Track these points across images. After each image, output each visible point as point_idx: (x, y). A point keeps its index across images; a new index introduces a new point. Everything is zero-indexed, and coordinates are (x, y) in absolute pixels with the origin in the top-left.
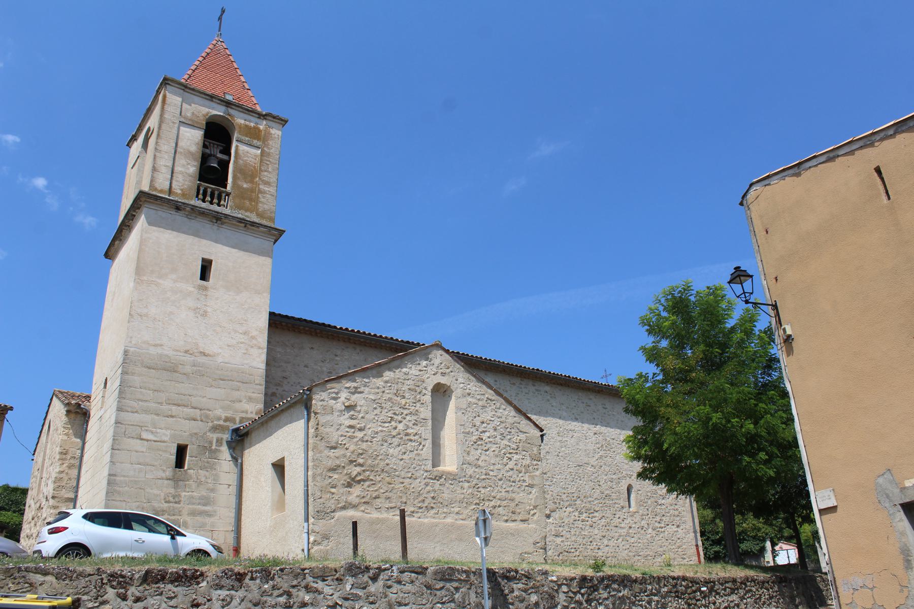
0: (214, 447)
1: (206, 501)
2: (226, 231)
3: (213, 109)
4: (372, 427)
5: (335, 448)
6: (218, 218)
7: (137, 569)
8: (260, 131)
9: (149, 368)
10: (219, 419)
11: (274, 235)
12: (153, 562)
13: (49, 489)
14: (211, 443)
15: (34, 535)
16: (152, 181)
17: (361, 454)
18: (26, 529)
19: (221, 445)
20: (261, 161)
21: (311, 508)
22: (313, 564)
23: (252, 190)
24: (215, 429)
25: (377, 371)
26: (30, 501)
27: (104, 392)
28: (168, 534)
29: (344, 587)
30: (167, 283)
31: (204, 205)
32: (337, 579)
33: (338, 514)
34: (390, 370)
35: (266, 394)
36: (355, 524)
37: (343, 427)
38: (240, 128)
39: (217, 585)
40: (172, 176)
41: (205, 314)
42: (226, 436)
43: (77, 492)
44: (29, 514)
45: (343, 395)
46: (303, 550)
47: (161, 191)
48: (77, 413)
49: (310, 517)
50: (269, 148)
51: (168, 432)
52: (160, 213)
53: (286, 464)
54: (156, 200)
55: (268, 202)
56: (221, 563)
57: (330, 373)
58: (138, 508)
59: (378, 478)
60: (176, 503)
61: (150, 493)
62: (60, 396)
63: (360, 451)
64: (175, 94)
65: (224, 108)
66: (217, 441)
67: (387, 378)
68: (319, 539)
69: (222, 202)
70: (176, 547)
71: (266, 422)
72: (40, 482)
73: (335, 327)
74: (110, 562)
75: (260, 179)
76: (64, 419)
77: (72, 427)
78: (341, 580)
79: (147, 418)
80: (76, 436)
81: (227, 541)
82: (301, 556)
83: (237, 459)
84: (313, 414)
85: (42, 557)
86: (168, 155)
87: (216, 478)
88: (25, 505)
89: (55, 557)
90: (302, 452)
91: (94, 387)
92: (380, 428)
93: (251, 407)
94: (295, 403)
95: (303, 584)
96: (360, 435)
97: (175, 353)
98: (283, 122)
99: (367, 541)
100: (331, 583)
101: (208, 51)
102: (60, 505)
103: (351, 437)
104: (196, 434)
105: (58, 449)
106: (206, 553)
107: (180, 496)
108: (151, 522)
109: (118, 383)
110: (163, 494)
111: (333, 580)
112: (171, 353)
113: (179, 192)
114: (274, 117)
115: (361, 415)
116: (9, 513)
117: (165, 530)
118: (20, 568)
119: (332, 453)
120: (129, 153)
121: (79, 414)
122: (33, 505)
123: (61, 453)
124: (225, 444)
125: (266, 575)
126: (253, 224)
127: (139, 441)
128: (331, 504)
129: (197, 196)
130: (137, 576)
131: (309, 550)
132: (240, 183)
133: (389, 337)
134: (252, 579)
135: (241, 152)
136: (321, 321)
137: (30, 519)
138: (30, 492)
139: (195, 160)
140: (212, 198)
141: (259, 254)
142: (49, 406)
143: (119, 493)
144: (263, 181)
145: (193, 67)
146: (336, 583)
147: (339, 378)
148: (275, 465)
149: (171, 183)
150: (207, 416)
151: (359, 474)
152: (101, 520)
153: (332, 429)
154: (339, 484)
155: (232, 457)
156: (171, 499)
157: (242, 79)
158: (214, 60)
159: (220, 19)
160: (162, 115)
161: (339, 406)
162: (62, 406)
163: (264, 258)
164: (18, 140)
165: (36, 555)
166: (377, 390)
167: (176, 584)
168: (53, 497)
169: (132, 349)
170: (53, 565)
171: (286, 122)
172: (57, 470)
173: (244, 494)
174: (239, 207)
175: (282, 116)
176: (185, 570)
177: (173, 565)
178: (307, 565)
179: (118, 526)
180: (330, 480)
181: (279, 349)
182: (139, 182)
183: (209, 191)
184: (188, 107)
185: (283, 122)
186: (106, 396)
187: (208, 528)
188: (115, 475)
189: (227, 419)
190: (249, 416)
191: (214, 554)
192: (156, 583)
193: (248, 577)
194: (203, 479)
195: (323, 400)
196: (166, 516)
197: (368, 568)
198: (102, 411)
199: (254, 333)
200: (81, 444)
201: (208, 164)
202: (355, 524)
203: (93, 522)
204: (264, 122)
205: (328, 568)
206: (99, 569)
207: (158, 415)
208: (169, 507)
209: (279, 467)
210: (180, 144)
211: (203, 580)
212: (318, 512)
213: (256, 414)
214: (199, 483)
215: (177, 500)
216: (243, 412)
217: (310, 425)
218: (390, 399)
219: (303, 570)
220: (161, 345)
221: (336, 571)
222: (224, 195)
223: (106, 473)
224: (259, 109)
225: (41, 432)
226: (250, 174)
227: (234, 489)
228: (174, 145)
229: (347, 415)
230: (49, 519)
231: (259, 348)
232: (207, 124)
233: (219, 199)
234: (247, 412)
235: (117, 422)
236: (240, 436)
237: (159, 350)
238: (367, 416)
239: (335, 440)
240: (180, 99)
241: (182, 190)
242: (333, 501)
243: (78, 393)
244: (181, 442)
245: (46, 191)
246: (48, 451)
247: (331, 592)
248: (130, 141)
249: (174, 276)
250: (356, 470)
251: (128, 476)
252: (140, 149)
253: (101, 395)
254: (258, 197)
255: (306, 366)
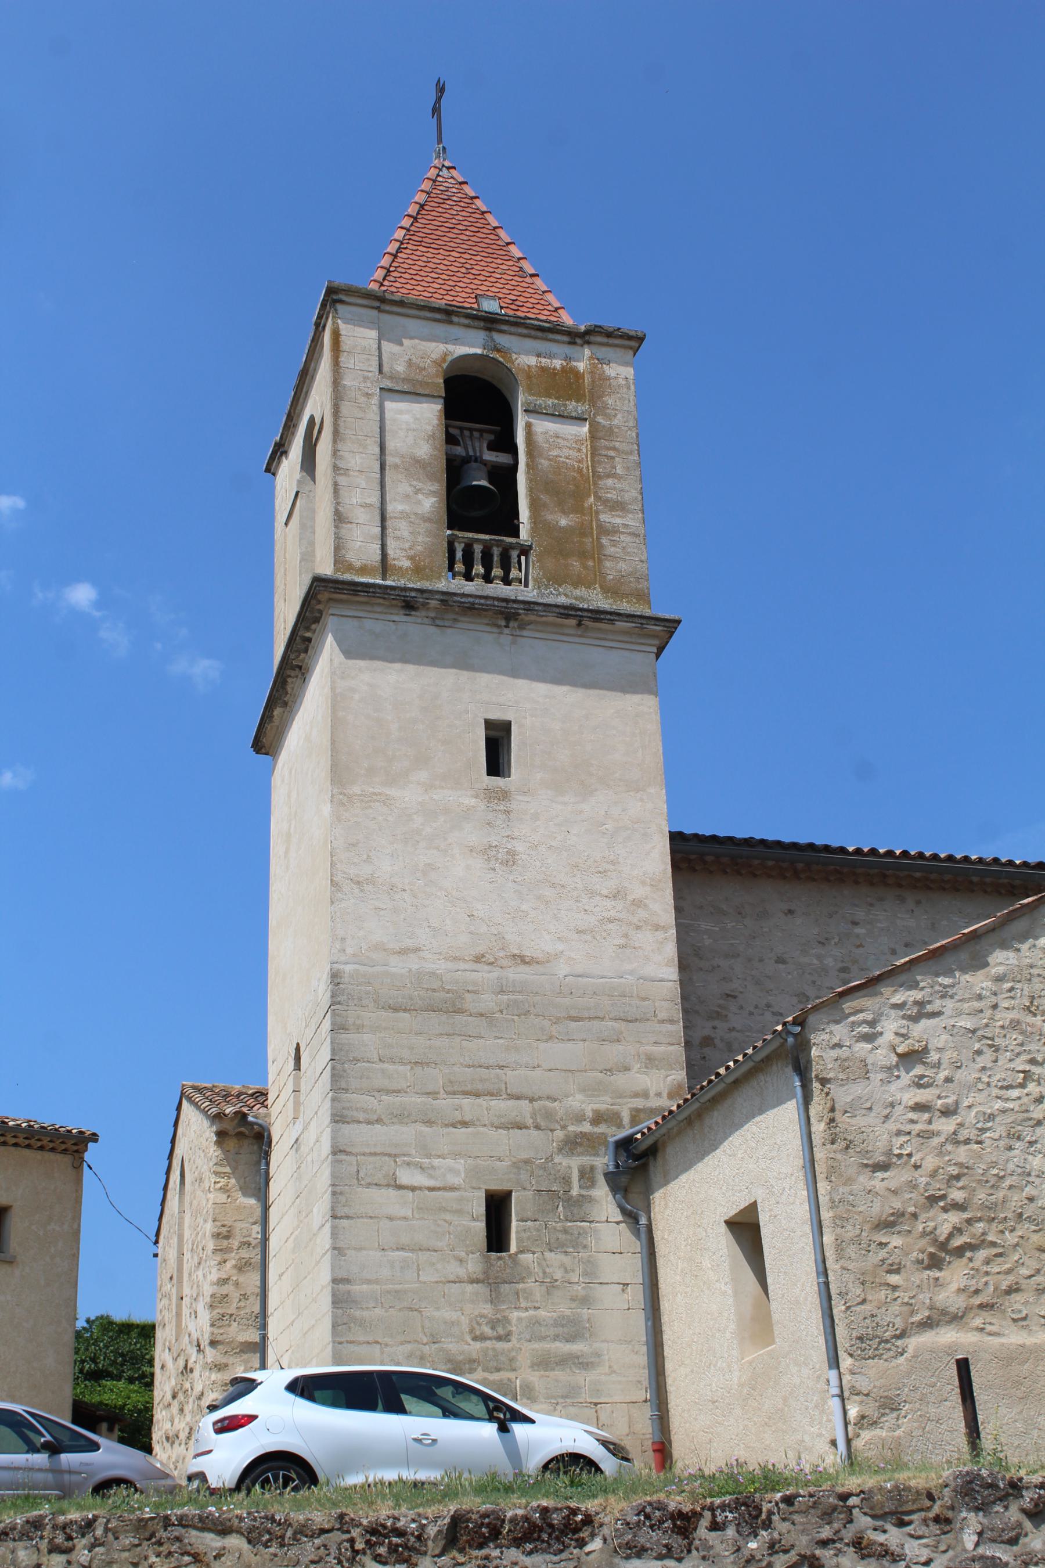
0: (575, 1191)
1: (573, 1329)
2: (534, 645)
3: (456, 341)
4: (977, 1104)
5: (884, 1167)
6: (509, 615)
7: (430, 1511)
8: (578, 375)
9: (395, 1010)
10: (580, 1118)
11: (655, 636)
12: (465, 1493)
13: (200, 1324)
14: (567, 1181)
15: (183, 1436)
16: (337, 549)
17: (957, 1178)
18: (163, 1423)
19: (592, 1183)
20: (594, 452)
21: (841, 1331)
22: (869, 1482)
23: (583, 531)
24: (573, 1144)
25: (970, 951)
26: (161, 1354)
27: (297, 1081)
28: (491, 1419)
29: (959, 1541)
30: (409, 795)
31: (470, 587)
32: (937, 1519)
33: (913, 1343)
34: (1004, 946)
35: (688, 1044)
36: (963, 1367)
37: (899, 1110)
38: (529, 377)
39: (628, 1546)
40: (383, 528)
41: (511, 860)
42: (603, 1161)
43: (264, 1326)
44: (163, 1386)
45: (890, 1026)
46: (834, 1443)
47: (363, 570)
48: (240, 1135)
49: (841, 1354)
50: (609, 417)
51: (460, 1164)
52: (369, 624)
53: (763, 1219)
54: (355, 592)
55: (626, 554)
56: (633, 1489)
57: (844, 970)
58: (409, 1358)
59: (1011, 1238)
60: (499, 1338)
61: (435, 1324)
62: (197, 1097)
63: (954, 1170)
64: (360, 322)
65: (482, 335)
66: (582, 1174)
67: (1001, 969)
68: (872, 1411)
69: (514, 573)
70: (513, 1452)
71: (700, 1115)
72: (179, 1307)
73: (843, 850)
74: (364, 1498)
75: (598, 498)
76: (214, 1152)
77: (234, 1170)
78: (948, 1521)
79: (406, 1134)
80: (245, 1191)
81: (635, 1427)
82: (833, 1460)
83: (636, 1217)
84: (816, 1085)
85: (213, 1492)
86: (366, 481)
87: (590, 1270)
88: (151, 1362)
89: (238, 1488)
90: (802, 1185)
91: (272, 1070)
92: (998, 1105)
93: (653, 1080)
94: (768, 1060)
95: (848, 1535)
96: (946, 1126)
97: (450, 965)
98: (633, 341)
99: (1003, 1410)
100: (922, 1530)
101: (421, 198)
102: (231, 1360)
103: (925, 1135)
104: (527, 1162)
105: (209, 1227)
106: (590, 1464)
107: (506, 1320)
108: (446, 1392)
109: (325, 1054)
110: (465, 1321)
111: (925, 1521)
112: (441, 967)
113: (406, 564)
114: (609, 335)
115: (942, 1075)
116: (121, 1384)
117: (481, 1409)
118: (167, 1518)
119: (879, 1181)
120: (274, 488)
121: (246, 1138)
122: (170, 1364)
123: (217, 1236)
124: (601, 1181)
125: (751, 1515)
126: (598, 615)
127: (392, 1192)
128: (893, 1316)
129: (451, 568)
130: (432, 1531)
131: (848, 1442)
132: (550, 517)
133: (989, 856)
134: (715, 1526)
135: (540, 439)
136: (803, 840)
137: (169, 1396)
138: (159, 1334)
139: (431, 477)
140: (488, 565)
141: (624, 690)
142: (176, 1124)
143: (362, 1323)
144: (605, 502)
145: (392, 248)
146: (935, 1529)
147: (872, 984)
148: (732, 1224)
149: (383, 547)
150: (549, 1115)
151: (958, 1230)
152: (328, 1393)
153: (871, 1119)
154: (908, 1261)
155: (624, 1211)
156: (487, 1330)
157: (515, 251)
158: (441, 219)
159: (436, 110)
160: (336, 382)
161: (882, 1055)
162: (206, 1123)
163: (636, 698)
164: (20, 503)
165: (196, 1484)
166: (977, 1005)
167: (529, 1546)
168: (213, 1343)
169: (348, 968)
170: (237, 1508)
171: (641, 339)
172: (214, 1276)
173: (665, 1305)
174: (557, 579)
175: (629, 326)
176: (545, 1511)
177: (515, 1499)
178: (852, 1483)
179: (368, 1405)
180: (882, 1254)
181: (704, 925)
182: (308, 557)
183: (478, 549)
184: (396, 349)
185: (633, 341)
186: (303, 1088)
187: (585, 1396)
188: (346, 1281)
189: (598, 1118)
190: (654, 1103)
191: (608, 1464)
192: (481, 1546)
193: (705, 1522)
194: (558, 1275)
195: (838, 1045)
196: (480, 1374)
197: (1016, 1487)
198: (299, 1126)
199: (639, 891)
200: (258, 1212)
201: (464, 484)
202: (963, 1367)
203: (311, 1398)
204: (587, 352)
205: (908, 1489)
206: (341, 1516)
207: (429, 1123)
208: (485, 1352)
209: (746, 1229)
210: (390, 445)
211: (593, 1535)
212: (860, 1339)
213: (671, 1096)
214: (551, 1286)
215: (501, 1331)
216: (636, 1095)
217: (812, 1112)
218: (1015, 1024)
219: (844, 1497)
220: (417, 950)
221: (930, 1497)
222: (514, 554)
223: (325, 1276)
224: (567, 319)
225: (165, 1188)
226: (571, 490)
227: (636, 1295)
228: (377, 450)
229: (906, 1078)
230: (211, 1397)
231: (657, 927)
232: (448, 382)
233: (506, 567)
234: (645, 1095)
235: (336, 1151)
236: (637, 1158)
237: (413, 963)
238: (959, 1075)
239: (881, 1145)
240: (373, 334)
241: (411, 558)
242: (895, 1308)
243: (237, 1087)
244: (494, 1186)
245: (97, 614)
246: (187, 1233)
247: (924, 1554)
248: (272, 458)
249: (423, 775)
250: (946, 1222)
251: (377, 1282)
252: (297, 474)
253: (290, 1087)
254: (601, 546)
255: (780, 960)
